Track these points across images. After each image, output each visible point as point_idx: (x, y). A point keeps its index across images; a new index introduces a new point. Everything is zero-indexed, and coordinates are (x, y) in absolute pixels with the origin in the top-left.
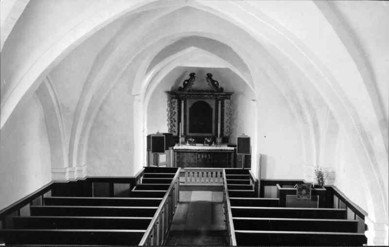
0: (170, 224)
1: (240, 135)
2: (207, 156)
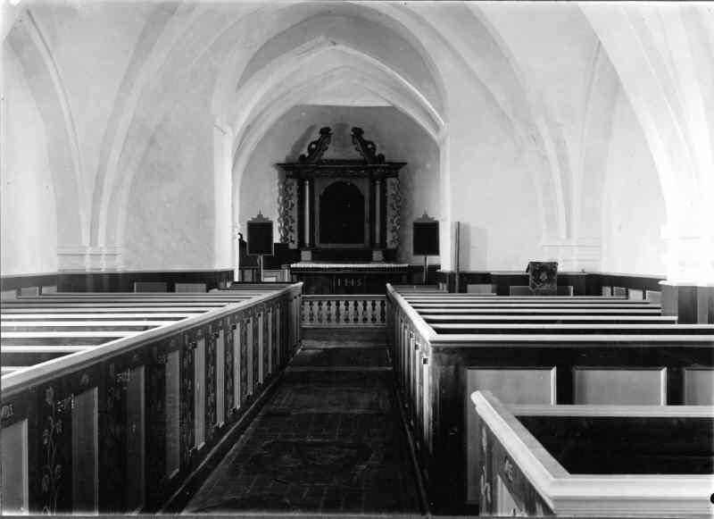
0: (285, 362)
1: (417, 216)
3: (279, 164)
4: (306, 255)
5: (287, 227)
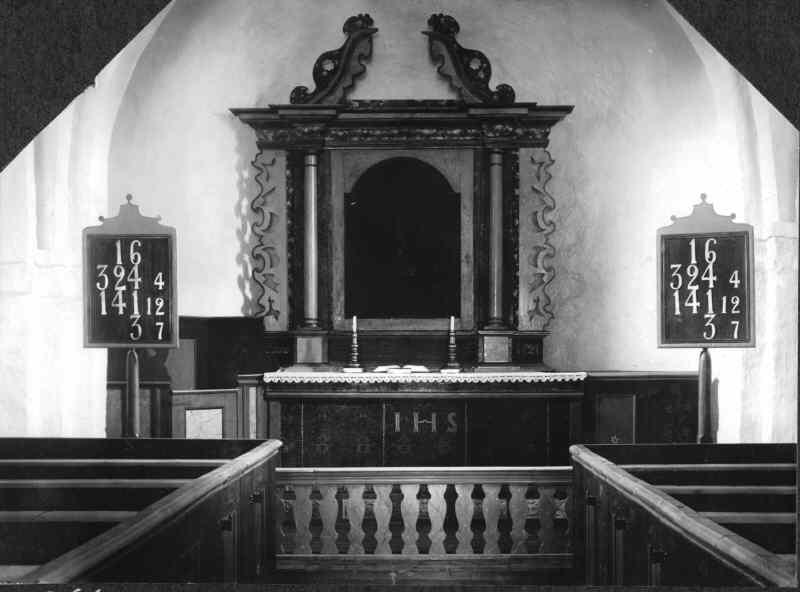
2: (442, 424)
3: (237, 112)
4: (310, 346)
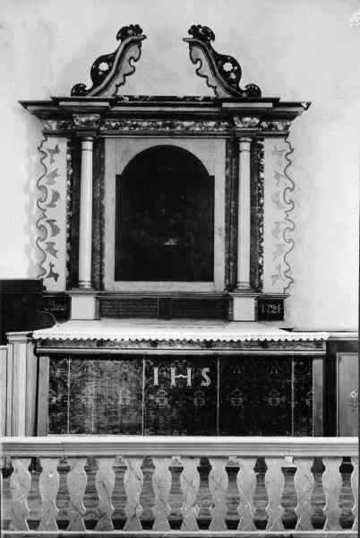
5: (43, 245)
